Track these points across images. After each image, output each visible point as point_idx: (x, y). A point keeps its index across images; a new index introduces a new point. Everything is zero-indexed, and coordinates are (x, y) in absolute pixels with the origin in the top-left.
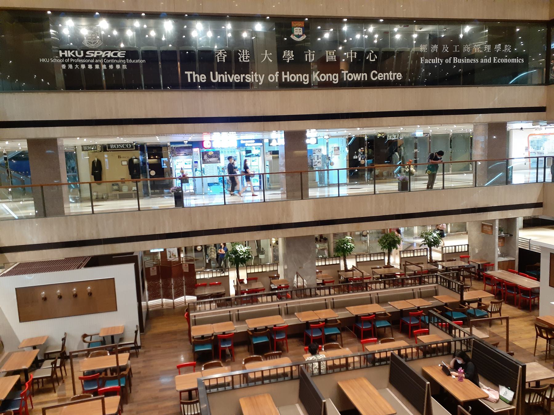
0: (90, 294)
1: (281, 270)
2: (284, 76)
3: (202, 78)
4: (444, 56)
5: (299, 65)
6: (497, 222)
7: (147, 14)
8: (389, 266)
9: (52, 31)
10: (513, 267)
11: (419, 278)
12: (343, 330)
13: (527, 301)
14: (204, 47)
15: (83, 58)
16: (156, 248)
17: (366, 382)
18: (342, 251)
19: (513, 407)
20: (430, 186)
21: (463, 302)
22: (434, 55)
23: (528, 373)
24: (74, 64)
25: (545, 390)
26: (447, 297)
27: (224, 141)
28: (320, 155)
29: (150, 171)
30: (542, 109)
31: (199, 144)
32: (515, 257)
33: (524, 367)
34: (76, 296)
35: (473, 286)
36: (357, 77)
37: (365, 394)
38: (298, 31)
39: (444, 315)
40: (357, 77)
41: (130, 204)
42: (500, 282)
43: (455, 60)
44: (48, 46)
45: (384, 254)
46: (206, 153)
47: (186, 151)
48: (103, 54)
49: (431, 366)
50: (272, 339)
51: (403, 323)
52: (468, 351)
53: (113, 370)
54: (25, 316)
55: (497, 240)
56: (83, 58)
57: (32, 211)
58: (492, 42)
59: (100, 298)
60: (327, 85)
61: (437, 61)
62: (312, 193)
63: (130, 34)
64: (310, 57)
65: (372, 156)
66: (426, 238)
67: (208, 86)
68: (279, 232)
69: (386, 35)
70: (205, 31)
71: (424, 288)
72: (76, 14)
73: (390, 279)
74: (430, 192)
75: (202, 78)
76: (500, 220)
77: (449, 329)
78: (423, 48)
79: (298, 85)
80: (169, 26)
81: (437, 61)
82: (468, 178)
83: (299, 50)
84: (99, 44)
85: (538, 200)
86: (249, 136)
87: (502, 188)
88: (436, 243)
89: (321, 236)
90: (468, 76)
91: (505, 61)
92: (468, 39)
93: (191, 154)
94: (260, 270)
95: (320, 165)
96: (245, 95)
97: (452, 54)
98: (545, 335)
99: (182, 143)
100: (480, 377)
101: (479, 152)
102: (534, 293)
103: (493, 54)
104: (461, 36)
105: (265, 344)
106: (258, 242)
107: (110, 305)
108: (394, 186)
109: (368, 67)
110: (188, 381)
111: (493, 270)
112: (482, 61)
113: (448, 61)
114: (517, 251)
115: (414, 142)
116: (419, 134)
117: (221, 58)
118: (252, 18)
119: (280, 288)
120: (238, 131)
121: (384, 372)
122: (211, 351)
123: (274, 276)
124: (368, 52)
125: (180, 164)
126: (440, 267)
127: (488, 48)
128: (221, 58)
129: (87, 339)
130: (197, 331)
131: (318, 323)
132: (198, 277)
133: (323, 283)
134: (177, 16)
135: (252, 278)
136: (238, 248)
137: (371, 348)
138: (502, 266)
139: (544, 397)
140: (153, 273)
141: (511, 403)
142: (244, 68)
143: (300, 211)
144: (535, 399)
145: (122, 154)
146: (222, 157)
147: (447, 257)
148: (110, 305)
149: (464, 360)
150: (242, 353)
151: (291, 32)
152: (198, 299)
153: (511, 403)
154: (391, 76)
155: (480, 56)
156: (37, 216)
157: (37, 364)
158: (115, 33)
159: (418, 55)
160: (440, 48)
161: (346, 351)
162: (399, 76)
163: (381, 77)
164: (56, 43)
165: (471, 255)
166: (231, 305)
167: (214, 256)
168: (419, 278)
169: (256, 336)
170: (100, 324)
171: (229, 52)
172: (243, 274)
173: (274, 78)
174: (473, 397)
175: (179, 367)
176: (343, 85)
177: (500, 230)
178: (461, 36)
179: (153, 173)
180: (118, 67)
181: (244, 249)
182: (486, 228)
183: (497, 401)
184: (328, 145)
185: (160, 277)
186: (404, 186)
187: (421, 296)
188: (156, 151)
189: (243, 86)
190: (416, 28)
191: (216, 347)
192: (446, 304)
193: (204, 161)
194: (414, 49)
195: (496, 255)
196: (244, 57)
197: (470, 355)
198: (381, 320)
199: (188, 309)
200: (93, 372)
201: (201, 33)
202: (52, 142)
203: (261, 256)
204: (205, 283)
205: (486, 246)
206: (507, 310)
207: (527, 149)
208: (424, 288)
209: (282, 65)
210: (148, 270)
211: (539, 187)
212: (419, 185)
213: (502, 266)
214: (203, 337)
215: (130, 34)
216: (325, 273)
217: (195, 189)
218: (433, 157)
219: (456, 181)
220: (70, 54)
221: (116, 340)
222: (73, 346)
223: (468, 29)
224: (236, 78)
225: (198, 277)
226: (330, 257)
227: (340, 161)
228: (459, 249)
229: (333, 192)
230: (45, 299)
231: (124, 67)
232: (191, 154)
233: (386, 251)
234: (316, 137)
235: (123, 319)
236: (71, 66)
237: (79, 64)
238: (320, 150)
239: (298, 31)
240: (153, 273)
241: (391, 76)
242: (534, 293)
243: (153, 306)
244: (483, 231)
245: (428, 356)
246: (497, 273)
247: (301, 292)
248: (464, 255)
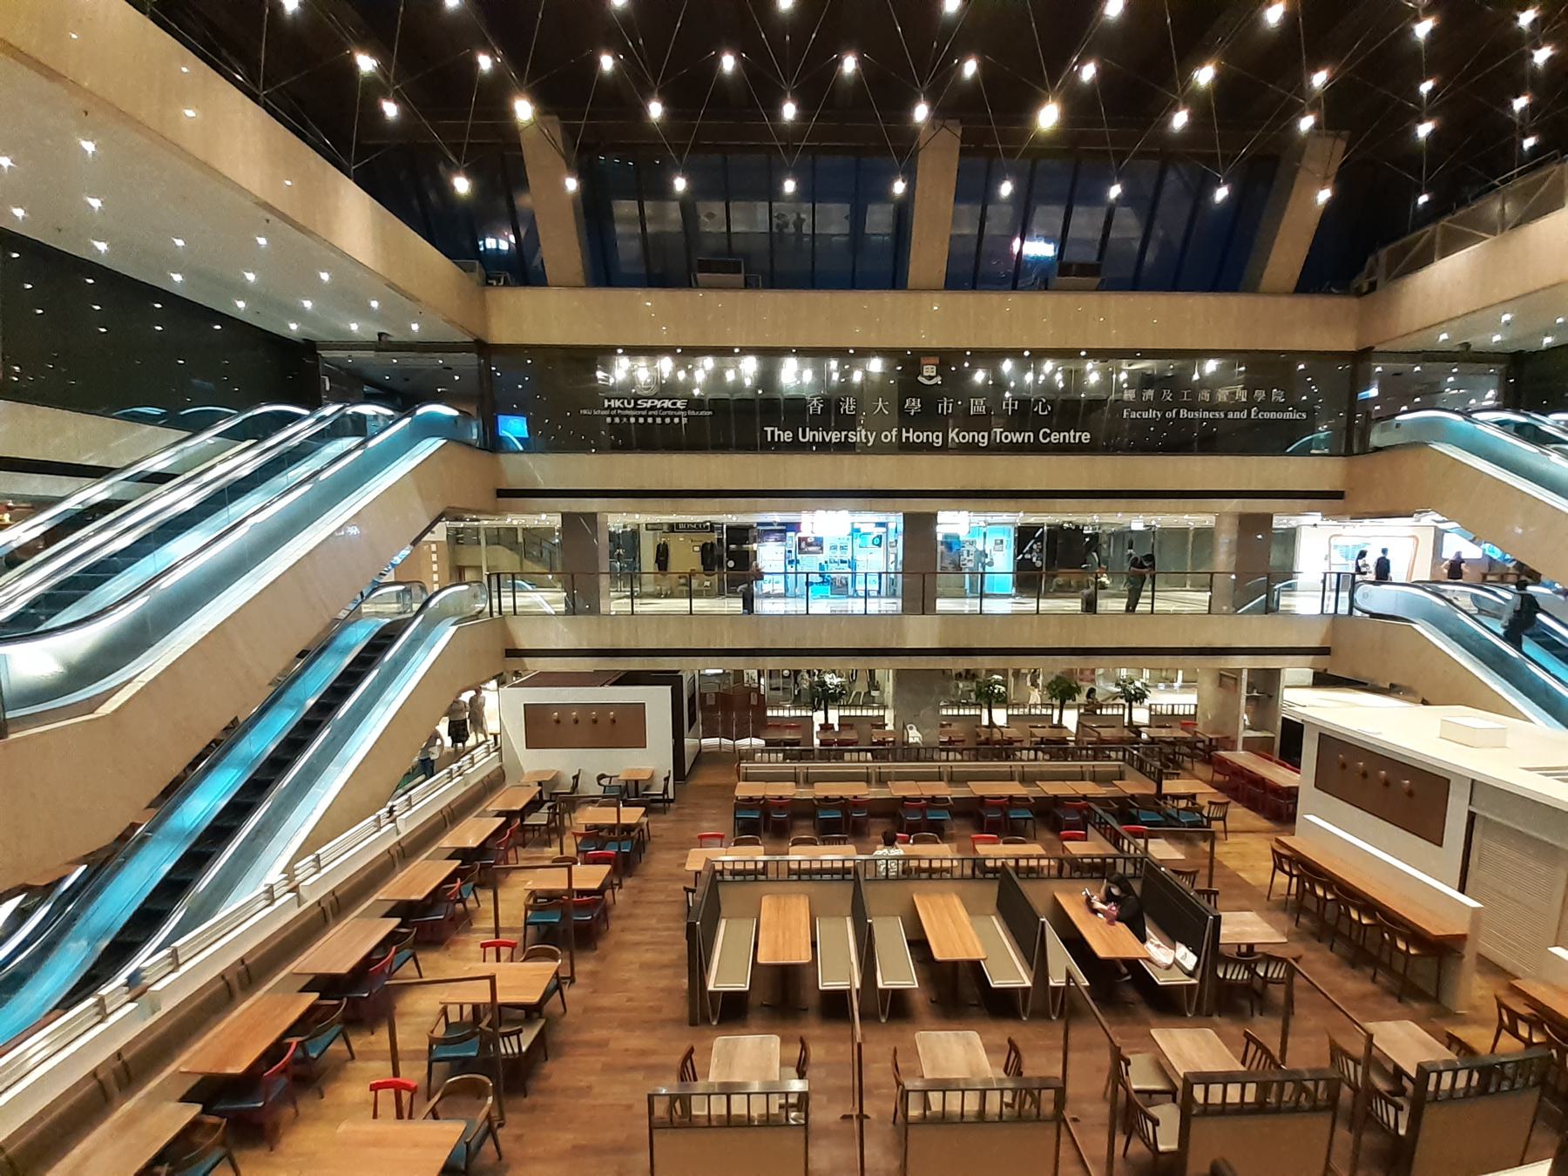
0: (614, 721)
1: (889, 716)
2: (904, 435)
3: (787, 436)
4: (1163, 406)
5: (929, 418)
6: (1245, 673)
7: (683, 348)
8: (1060, 726)
9: (600, 374)
10: (1270, 749)
11: (1100, 749)
12: (956, 814)
13: (1279, 807)
14: (792, 393)
15: (634, 408)
16: (713, 668)
17: (957, 901)
18: (990, 699)
19: (1194, 981)
20: (1131, 608)
21: (1160, 796)
22: (1148, 406)
23: (1223, 930)
24: (621, 417)
25: (1256, 962)
26: (1135, 786)
27: (827, 524)
28: (972, 549)
29: (730, 562)
30: (1337, 495)
31: (794, 527)
32: (1276, 733)
33: (1218, 920)
34: (595, 721)
35: (1196, 772)
36: (1017, 437)
37: (949, 920)
38: (929, 370)
39: (1126, 815)
40: (1017, 437)
41: (681, 605)
42: (1239, 772)
43: (1183, 413)
44: (596, 390)
45: (1053, 707)
46: (805, 539)
47: (778, 535)
48: (658, 404)
49: (1069, 892)
50: (847, 816)
51: (1053, 817)
52: (1134, 877)
53: (611, 828)
54: (535, 739)
55: (1243, 701)
56: (634, 408)
57: (562, 607)
58: (1250, 388)
59: (623, 728)
60: (971, 449)
61: (1152, 414)
62: (942, 605)
63: (700, 376)
64: (946, 406)
65: (1052, 558)
66: (1124, 689)
67: (796, 447)
68: (886, 660)
69: (1074, 377)
70: (799, 375)
71: (1101, 765)
72: (633, 351)
73: (1056, 746)
74: (1130, 617)
75: (787, 436)
76: (1250, 670)
77: (1115, 839)
78: (1129, 395)
79: (927, 448)
80: (749, 367)
81: (1152, 414)
82: (1198, 600)
83: (930, 397)
84: (654, 390)
85: (1323, 641)
86: (868, 520)
87: (1257, 620)
88: (1140, 696)
89: (968, 671)
90: (1209, 441)
91: (1273, 415)
92: (1209, 383)
93: (783, 539)
94: (955, 712)
95: (971, 565)
96: (847, 460)
97: (1177, 404)
98: (1287, 868)
99: (770, 524)
100: (1147, 920)
101: (1223, 558)
102: (1292, 794)
103: (1248, 406)
104: (1196, 377)
105: (841, 822)
106: (872, 673)
107: (637, 739)
108: (1075, 605)
109: (1035, 424)
110: (730, 856)
111: (1233, 748)
112: (1230, 416)
113: (1171, 415)
114: (1279, 723)
115: (1124, 537)
116: (1137, 525)
117: (815, 410)
118: (864, 353)
119: (883, 743)
120: (853, 511)
121: (992, 890)
122: (764, 822)
123: (879, 723)
124: (1037, 401)
125: (769, 555)
126: (1144, 736)
127: (1242, 396)
128: (815, 410)
129: (605, 782)
130: (744, 790)
131: (919, 800)
132: (769, 713)
133: (950, 742)
134: (1064, 353)
135: (845, 723)
136: (828, 678)
137: (983, 849)
138: (1249, 745)
139: (1253, 972)
140: (711, 701)
141: (1191, 974)
142: (849, 423)
143: (920, 632)
144: (1237, 974)
145: (694, 536)
146: (826, 546)
147: (1158, 719)
148: (637, 739)
149: (1122, 890)
150: (878, 828)
151: (920, 373)
152: (767, 744)
153: (1191, 974)
154: (1071, 436)
155: (1226, 408)
156: (567, 613)
157: (534, 805)
158: (682, 375)
159: (1120, 404)
160: (1158, 395)
161: (1035, 849)
162: (1086, 437)
163: (1055, 437)
164: (607, 388)
165: (1200, 722)
166: (813, 760)
167: (805, 685)
168: (1100, 749)
169: (826, 809)
170: (625, 763)
171: (826, 401)
172: (834, 716)
173: (890, 436)
174: (1131, 954)
175: (701, 837)
176: (996, 448)
177: (1251, 687)
178: (1196, 377)
179: (731, 564)
180: (650, 420)
181: (836, 681)
182: (1226, 680)
183: (1168, 968)
184: (982, 535)
185: (719, 708)
186: (1090, 606)
187: (1096, 778)
188: (740, 534)
189: (846, 447)
190: (1124, 364)
191: (766, 815)
192: (1132, 797)
193: (801, 551)
194: (1113, 397)
195: (1241, 727)
196: (848, 407)
197: (1137, 887)
198: (1017, 807)
199: (749, 755)
200: (596, 827)
201: (793, 376)
202: (592, 518)
203: (874, 693)
204: (781, 724)
205: (1226, 713)
206: (1239, 814)
207: (1328, 558)
208: (1101, 765)
209: (905, 420)
210: (703, 696)
211: (1327, 621)
212: (1112, 605)
213: (1249, 745)
214: (751, 799)
215: (700, 376)
216: (955, 727)
217: (786, 590)
218: (1135, 563)
219: (1179, 603)
220: (618, 403)
221: (641, 787)
222: (592, 788)
223: (1211, 366)
224: (834, 436)
225: (769, 713)
226: (967, 705)
227: (1003, 560)
228: (1179, 711)
229: (857, 606)
230: (558, 722)
231: (684, 421)
232: (783, 539)
233: (1057, 702)
234: (953, 522)
235: (652, 759)
236: (617, 420)
237: (628, 417)
238: (972, 543)
239: (929, 370)
240: (711, 701)
241: (1071, 436)
242: (1292, 794)
243: (707, 747)
244: (1221, 685)
245: (1077, 874)
246: (1240, 757)
247: (914, 753)
248: (1187, 721)
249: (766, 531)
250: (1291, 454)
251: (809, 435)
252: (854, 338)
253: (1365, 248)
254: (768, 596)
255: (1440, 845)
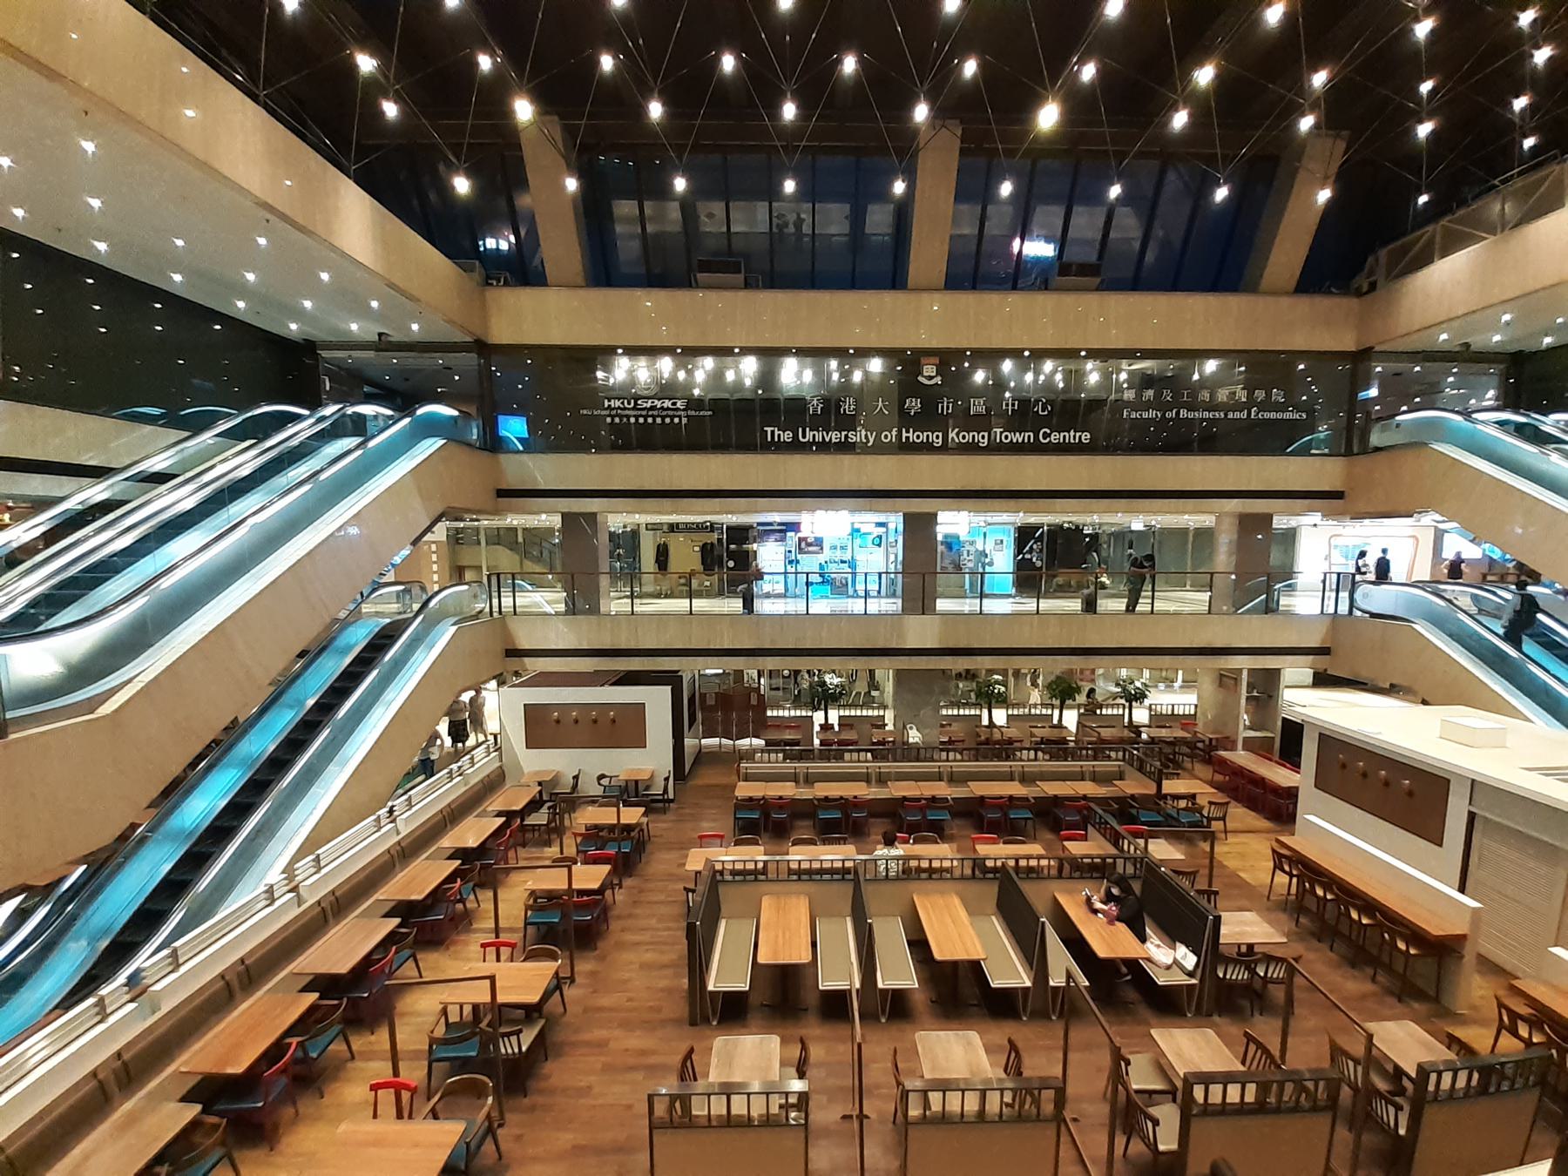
0: (614, 721)
1: (889, 716)
2: (904, 435)
3: (787, 436)
4: (1163, 406)
5: (929, 418)
6: (1245, 673)
7: (683, 348)
8: (1060, 726)
9: (600, 374)
10: (1270, 749)
11: (1100, 749)
12: (956, 814)
13: (1279, 807)
14: (792, 393)
15: (634, 408)
16: (713, 668)
17: (957, 901)
18: (990, 699)
19: (1194, 981)
20: (1131, 608)
21: (1160, 796)
22: (1148, 406)
23: (1223, 930)
24: (621, 417)
25: (1256, 962)
26: (1135, 786)
27: (827, 524)
28: (972, 549)
29: (730, 562)
30: (1337, 495)
31: (794, 527)
32: (1276, 733)
33: (1218, 920)
34: (595, 721)
35: (1196, 772)
36: (1017, 437)
37: (949, 920)
38: (929, 370)
39: (1126, 815)
40: (1017, 437)
41: (681, 605)
42: (1239, 772)
43: (1183, 413)
44: (596, 390)
45: (1053, 707)
46: (805, 539)
47: (778, 535)
48: (658, 404)
49: (1069, 892)
50: (847, 816)
51: (1053, 817)
52: (1134, 877)
53: (611, 828)
54: (535, 739)
55: (1243, 701)
56: (634, 408)
57: (562, 607)
58: (1250, 388)
59: (623, 728)
60: (971, 449)
61: (1152, 414)
62: (942, 605)
63: (700, 376)
64: (946, 406)
65: (1052, 558)
66: (1124, 689)
67: (796, 447)
68: (886, 660)
69: (1074, 377)
70: (799, 375)
71: (1101, 765)
72: (633, 351)
73: (1056, 746)
74: (1130, 617)
75: (787, 436)
76: (1250, 670)
77: (1115, 839)
78: (1129, 395)
79: (927, 448)
80: (749, 367)
81: (1152, 414)
82: (1198, 600)
83: (930, 397)
84: (654, 390)
85: (1323, 641)
86: (868, 520)
87: (1257, 620)
88: (1140, 696)
89: (968, 671)
90: (1209, 441)
91: (1273, 415)
92: (1209, 383)
93: (783, 539)
94: (955, 712)
95: (971, 565)
96: (847, 460)
97: (1177, 404)
98: (1287, 868)
99: (770, 524)
100: (1147, 920)
101: (1223, 558)
102: (1292, 794)
103: (1248, 406)
104: (1196, 377)
105: (841, 822)
106: (872, 673)
107: (637, 739)
108: (1075, 605)
109: (1035, 424)
110: (730, 856)
111: (1233, 748)
112: (1230, 416)
113: (1171, 415)
114: (1279, 723)
115: (1124, 537)
116: (1137, 525)
117: (815, 410)
118: (864, 353)
119: (883, 743)
120: (853, 511)
121: (992, 890)
122: (764, 822)
123: (879, 723)
124: (1037, 401)
125: (769, 555)
126: (1144, 736)
127: (1242, 396)
128: (815, 410)
129: (605, 782)
130: (744, 790)
131: (919, 800)
132: (769, 713)
133: (950, 742)
134: (1064, 353)
135: (845, 723)
136: (828, 678)
137: (983, 849)
138: (1249, 745)
139: (1253, 972)
140: (711, 701)
141: (1191, 974)
142: (849, 423)
143: (920, 632)
144: (1237, 974)
145: (694, 536)
146: (826, 546)
147: (1158, 719)
148: (637, 739)
149: (1122, 890)
150: (878, 828)
151: (920, 373)
152: (767, 744)
153: (1191, 974)
154: (1071, 436)
155: (1226, 408)
156: (567, 613)
157: (534, 805)
158: (682, 375)
159: (1120, 404)
160: (1158, 395)
161: (1035, 849)
162: (1086, 437)
163: (1055, 437)
164: (607, 388)
165: (1200, 722)
166: (813, 760)
167: (805, 685)
168: (1100, 749)
169: (826, 809)
170: (625, 763)
171: (826, 401)
172: (834, 716)
173: (890, 436)
174: (1131, 954)
175: (701, 837)
176: (996, 448)
177: (1251, 687)
178: (1196, 377)
179: (731, 564)
180: (650, 420)
181: (836, 681)
182: (1226, 680)
183: (1168, 968)
184: (982, 535)
185: (719, 708)
186: (1090, 606)
187: (1096, 778)
188: (740, 534)
189: (846, 447)
190: (1124, 364)
191: (766, 815)
192: (1132, 797)
193: (801, 551)
194: (1113, 397)
195: (1241, 727)
196: (848, 407)
197: (1137, 887)
198: (1017, 807)
199: (749, 755)
200: (596, 827)
201: (793, 376)
202: (592, 518)
203: (874, 693)
204: (781, 724)
205: (1226, 713)
206: (1239, 814)
207: (1328, 558)
208: (1101, 765)
209: (905, 420)
210: (703, 696)
211: (1327, 621)
212: (1112, 605)
213: (1249, 745)
214: (751, 799)
215: (700, 376)
216: (955, 727)
217: (786, 590)
218: (1135, 563)
219: (1179, 603)
220: (618, 403)
221: (641, 787)
222: (592, 788)
223: (1211, 366)
224: (834, 436)
225: (769, 713)
226: (967, 705)
227: (1003, 560)
228: (1179, 711)
229: (857, 606)
230: (558, 722)
231: (684, 421)
232: (783, 539)
233: (1057, 702)
234: (953, 522)
235: (652, 759)
236: (617, 420)
237: (628, 417)
238: (972, 543)
239: (929, 370)
240: (711, 701)
241: (1071, 436)
242: (1292, 794)
243: (707, 747)
244: (1221, 685)
245: (1077, 874)
246: (1240, 757)
247: (914, 753)
248: (1187, 721)
249: (766, 531)
250: (1291, 454)
251: (809, 435)
252: (854, 338)
253: (1365, 248)
254: (768, 596)
255: (1440, 845)
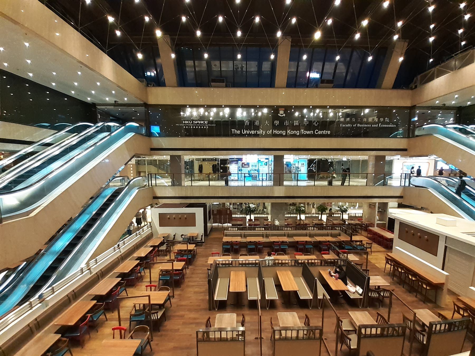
0: (186, 218)
1: (269, 217)
2: (274, 132)
3: (238, 132)
4: (352, 123)
5: (281, 126)
6: (377, 204)
7: (207, 105)
8: (321, 220)
9: (182, 113)
10: (385, 227)
11: (333, 227)
12: (290, 246)
13: (387, 244)
14: (240, 119)
15: (192, 124)
16: (216, 202)
17: (290, 273)
18: (300, 211)
19: (362, 297)
20: (343, 184)
21: (351, 241)
22: (348, 123)
23: (371, 282)
24: (188, 126)
25: (381, 291)
26: (344, 238)
27: (251, 159)
28: (294, 166)
29: (221, 170)
30: (405, 150)
31: (241, 159)
32: (386, 222)
33: (369, 278)
34: (180, 218)
35: (362, 234)
36: (308, 132)
37: (287, 279)
38: (281, 112)
39: (341, 247)
40: (308, 132)
41: (206, 183)
42: (375, 234)
43: (359, 125)
44: (180, 118)
45: (319, 214)
46: (244, 163)
47: (236, 162)
48: (199, 122)
49: (324, 270)
50: (257, 247)
51: (319, 247)
52: (344, 265)
53: (185, 251)
54: (162, 224)
55: (377, 212)
56: (192, 124)
57: (170, 184)
58: (379, 117)
59: (189, 221)
60: (294, 136)
61: (349, 125)
62: (285, 183)
63: (212, 114)
64: (286, 123)
65: (319, 169)
66: (341, 209)
67: (241, 135)
68: (268, 200)
69: (325, 114)
70: (242, 113)
71: (334, 232)
72: (192, 106)
73: (320, 226)
74: (342, 187)
75: (238, 132)
76: (379, 203)
77: (338, 254)
78: (342, 120)
79: (281, 136)
80: (227, 111)
81: (349, 125)
82: (363, 182)
83: (282, 120)
84: (198, 118)
85: (401, 194)
86: (263, 157)
87: (381, 188)
88: (345, 211)
89: (293, 203)
90: (366, 134)
91: (385, 126)
92: (366, 116)
93: (237, 163)
94: (289, 216)
95: (294, 171)
96: (257, 139)
97: (357, 122)
98: (390, 263)
99: (233, 159)
100: (348, 279)
101: (371, 169)
102: (391, 240)
103: (378, 123)
104: (362, 114)
105: (255, 249)
106: (264, 204)
107: (193, 224)
108: (326, 183)
109: (314, 128)
110: (221, 259)
111: (374, 227)
112: (373, 126)
113: (355, 125)
114: (388, 219)
115: (341, 163)
116: (345, 159)
117: (247, 124)
118: (262, 107)
119: (267, 225)
120: (258, 155)
121: (300, 269)
122: (232, 249)
123: (266, 219)
124: (314, 121)
125: (233, 168)
126: (347, 223)
127: (376, 120)
128: (247, 124)
129: (183, 237)
130: (225, 239)
131: (278, 242)
132: (233, 216)
133: (288, 225)
134: (322, 107)
135: (256, 219)
136: (251, 205)
137: (298, 257)
138: (378, 225)
139: (380, 294)
140: (215, 212)
141: (361, 295)
142: (257, 128)
143: (279, 191)
144: (375, 295)
145: (210, 162)
146: (250, 165)
147: (351, 218)
148: (193, 224)
149: (340, 269)
150: (266, 251)
151: (279, 113)
152: (232, 225)
153: (361, 295)
154: (325, 132)
155: (371, 123)
156: (172, 186)
157: (162, 244)
158: (206, 114)
159: (339, 122)
160: (351, 120)
161: (314, 257)
162: (329, 132)
163: (320, 132)
164: (184, 117)
165: (364, 219)
166: (246, 230)
167: (244, 207)
168: (333, 227)
169: (250, 245)
170: (189, 231)
171: (250, 121)
172: (253, 217)
173: (270, 132)
174: (343, 289)
175: (212, 253)
176: (302, 136)
177: (379, 208)
178: (362, 114)
179: (221, 171)
180: (197, 127)
181: (253, 206)
182: (371, 206)
183: (354, 293)
184: (298, 162)
185: (218, 214)
186: (330, 183)
187: (332, 235)
188: (224, 162)
189: (256, 135)
190: (341, 110)
191: (232, 247)
192: (343, 241)
193: (243, 167)
194: (337, 120)
195: (376, 220)
196: (257, 123)
197: (344, 268)
198: (308, 244)
199: (227, 228)
200: (181, 250)
201: (240, 114)
202: (179, 157)
203: (265, 210)
204: (237, 219)
205: (372, 216)
206: (375, 247)
207: (402, 169)
208: (334, 232)
209: (274, 127)
210: (213, 211)
211: (402, 188)
212: (337, 183)
213: (378, 225)
214: (227, 242)
215: (212, 114)
216: (289, 220)
217: (238, 178)
218: (344, 170)
219: (357, 183)
220: (187, 122)
221: (194, 238)
222: (179, 239)
223: (367, 111)
224: (253, 132)
225: (233, 216)
226: (293, 213)
227: (304, 170)
228: (357, 215)
229: (260, 183)
230: (169, 218)
231: (207, 127)
232: (237, 163)
233: (320, 213)
234: (289, 158)
235: (197, 230)
236: (187, 127)
237: (190, 126)
238: (295, 164)
239: (281, 112)
240: (215, 212)
241: (325, 132)
242: (391, 240)
243: (214, 226)
244: (370, 207)
245: (326, 265)
246: (376, 229)
247: (277, 228)
248: (360, 218)
249: (232, 161)
250: (391, 137)
251: (245, 132)
252: (259, 102)
253: (413, 75)
254: (233, 180)
255: (436, 256)
